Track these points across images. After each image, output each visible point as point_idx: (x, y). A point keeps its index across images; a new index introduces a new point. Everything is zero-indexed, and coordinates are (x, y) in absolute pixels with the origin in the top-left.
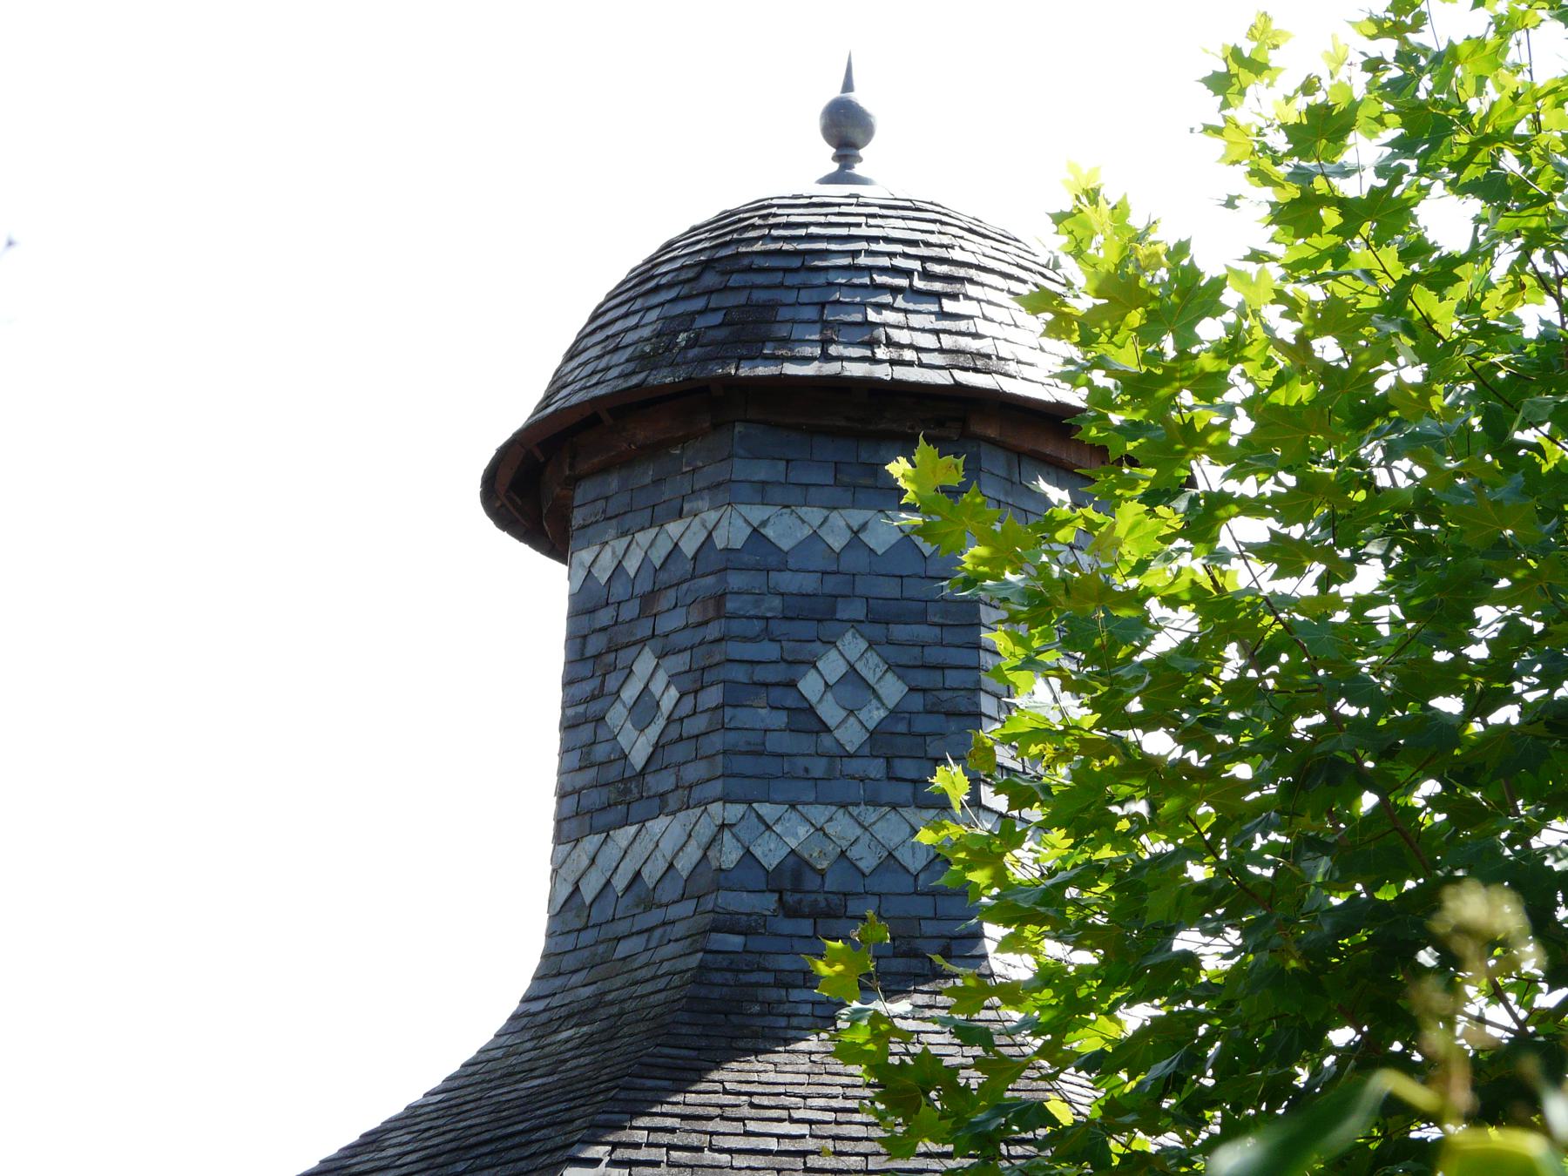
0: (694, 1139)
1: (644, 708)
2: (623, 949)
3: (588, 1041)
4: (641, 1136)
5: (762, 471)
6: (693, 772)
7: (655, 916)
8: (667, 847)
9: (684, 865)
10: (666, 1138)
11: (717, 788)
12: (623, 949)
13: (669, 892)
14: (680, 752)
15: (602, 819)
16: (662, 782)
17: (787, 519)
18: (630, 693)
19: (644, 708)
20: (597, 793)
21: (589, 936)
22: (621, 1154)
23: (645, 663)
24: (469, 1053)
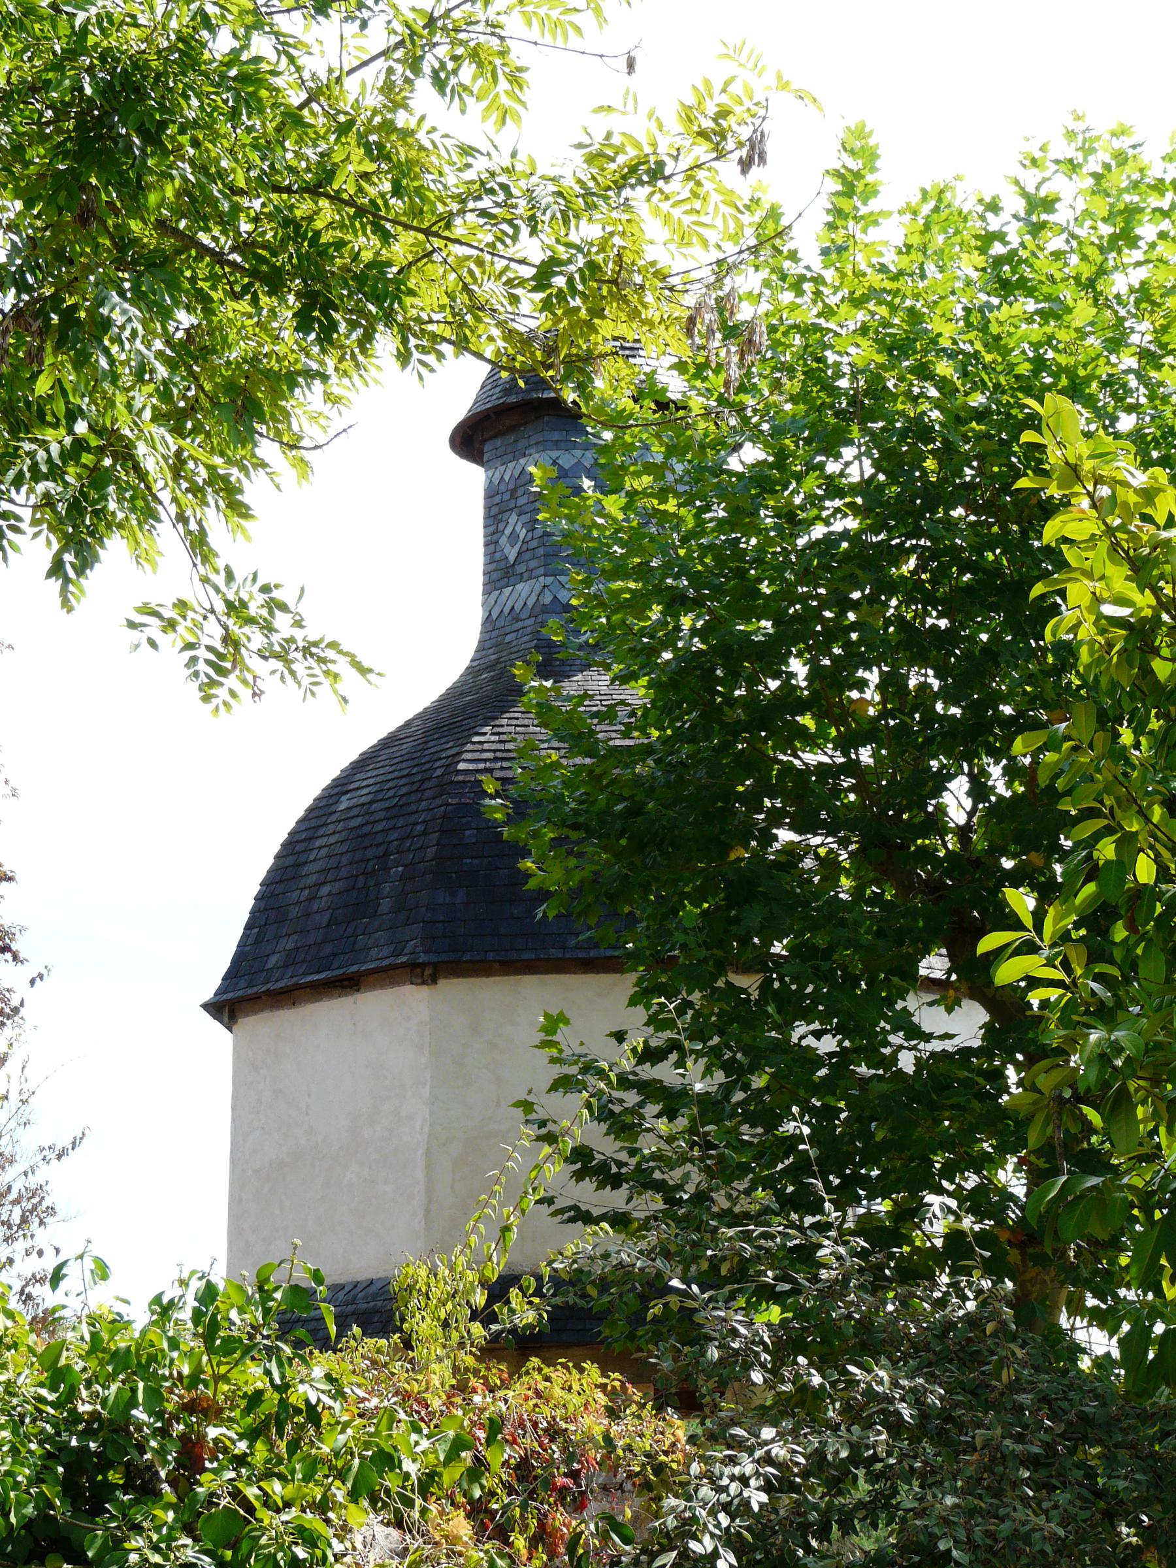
0: (526, 722)
1: (513, 536)
2: (508, 639)
3: (492, 679)
4: (504, 722)
5: (556, 436)
6: (533, 564)
7: (519, 625)
8: (524, 596)
9: (530, 603)
10: (515, 722)
11: (542, 570)
12: (508, 639)
13: (524, 615)
14: (528, 555)
15: (499, 584)
16: (521, 568)
17: (567, 455)
18: (508, 531)
19: (513, 536)
20: (499, 574)
21: (494, 634)
22: (496, 730)
23: (513, 518)
24: (449, 685)
